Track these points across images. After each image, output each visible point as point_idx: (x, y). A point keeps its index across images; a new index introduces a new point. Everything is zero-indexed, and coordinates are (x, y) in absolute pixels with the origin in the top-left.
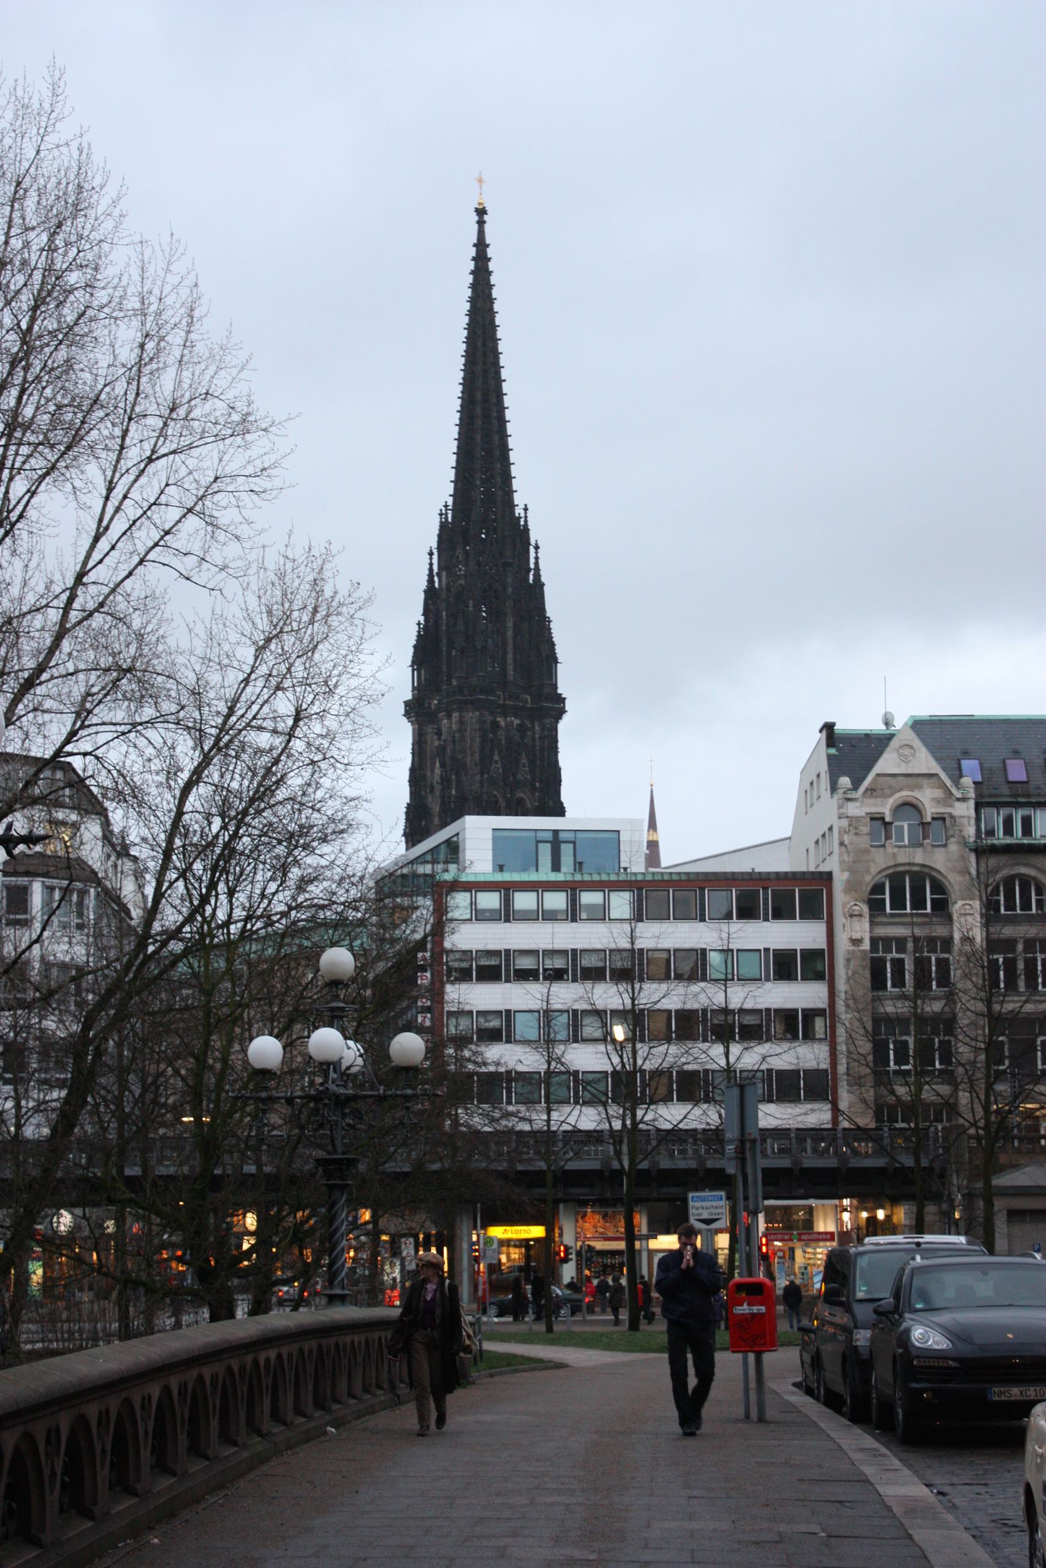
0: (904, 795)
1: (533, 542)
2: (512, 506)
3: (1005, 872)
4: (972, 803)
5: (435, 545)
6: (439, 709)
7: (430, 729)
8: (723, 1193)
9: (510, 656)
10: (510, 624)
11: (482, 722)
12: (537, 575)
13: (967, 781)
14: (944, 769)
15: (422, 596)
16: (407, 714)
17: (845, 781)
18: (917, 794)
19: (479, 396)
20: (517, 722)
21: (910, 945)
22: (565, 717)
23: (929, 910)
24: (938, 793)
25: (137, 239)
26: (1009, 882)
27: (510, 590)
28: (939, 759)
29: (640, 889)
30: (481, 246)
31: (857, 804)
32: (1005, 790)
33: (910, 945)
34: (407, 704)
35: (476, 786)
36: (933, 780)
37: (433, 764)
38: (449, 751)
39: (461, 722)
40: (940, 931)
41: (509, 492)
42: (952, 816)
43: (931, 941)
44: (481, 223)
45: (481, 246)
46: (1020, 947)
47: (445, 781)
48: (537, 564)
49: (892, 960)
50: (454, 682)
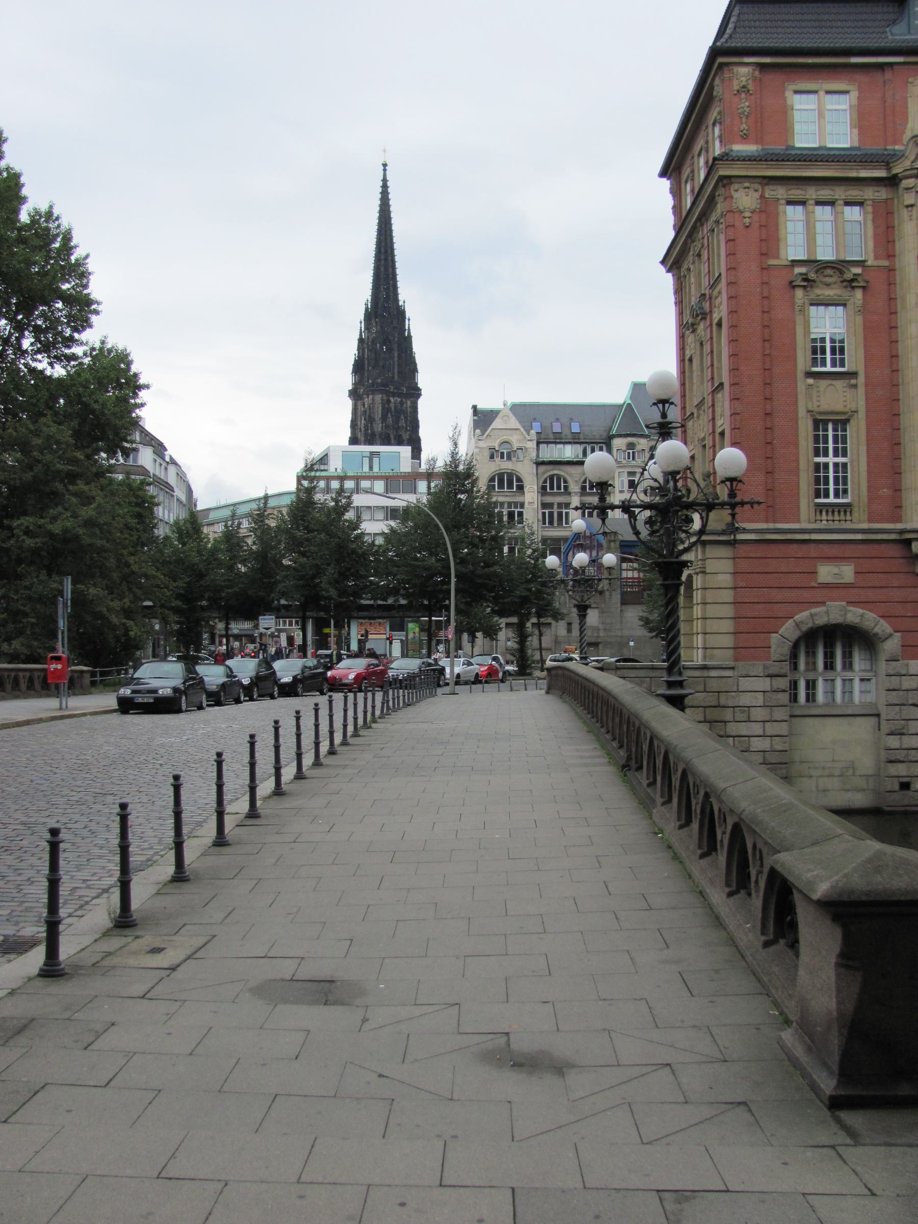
0: (505, 438)
1: (407, 317)
2: (397, 300)
3: (551, 473)
4: (535, 442)
5: (363, 319)
6: (363, 394)
7: (359, 403)
8: (273, 617)
9: (396, 370)
10: (396, 355)
11: (382, 400)
12: (409, 332)
13: (533, 432)
14: (524, 427)
15: (357, 342)
16: (350, 396)
17: (478, 431)
18: (510, 438)
19: (383, 250)
20: (399, 400)
21: (506, 506)
22: (421, 397)
23: (515, 490)
24: (519, 437)
25: (722, 120)
26: (551, 478)
27: (396, 339)
28: (520, 422)
29: (387, 479)
30: (385, 181)
31: (483, 442)
32: (551, 436)
33: (506, 506)
34: (350, 391)
35: (380, 429)
36: (517, 432)
37: (361, 419)
38: (368, 413)
39: (373, 400)
40: (518, 499)
41: (396, 294)
42: (526, 449)
43: (516, 504)
44: (385, 170)
45: (385, 181)
46: (555, 506)
47: (366, 426)
48: (409, 327)
49: (518, 512)
50: (370, 381)
